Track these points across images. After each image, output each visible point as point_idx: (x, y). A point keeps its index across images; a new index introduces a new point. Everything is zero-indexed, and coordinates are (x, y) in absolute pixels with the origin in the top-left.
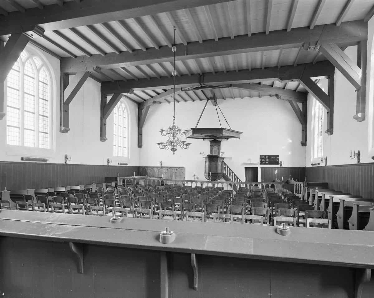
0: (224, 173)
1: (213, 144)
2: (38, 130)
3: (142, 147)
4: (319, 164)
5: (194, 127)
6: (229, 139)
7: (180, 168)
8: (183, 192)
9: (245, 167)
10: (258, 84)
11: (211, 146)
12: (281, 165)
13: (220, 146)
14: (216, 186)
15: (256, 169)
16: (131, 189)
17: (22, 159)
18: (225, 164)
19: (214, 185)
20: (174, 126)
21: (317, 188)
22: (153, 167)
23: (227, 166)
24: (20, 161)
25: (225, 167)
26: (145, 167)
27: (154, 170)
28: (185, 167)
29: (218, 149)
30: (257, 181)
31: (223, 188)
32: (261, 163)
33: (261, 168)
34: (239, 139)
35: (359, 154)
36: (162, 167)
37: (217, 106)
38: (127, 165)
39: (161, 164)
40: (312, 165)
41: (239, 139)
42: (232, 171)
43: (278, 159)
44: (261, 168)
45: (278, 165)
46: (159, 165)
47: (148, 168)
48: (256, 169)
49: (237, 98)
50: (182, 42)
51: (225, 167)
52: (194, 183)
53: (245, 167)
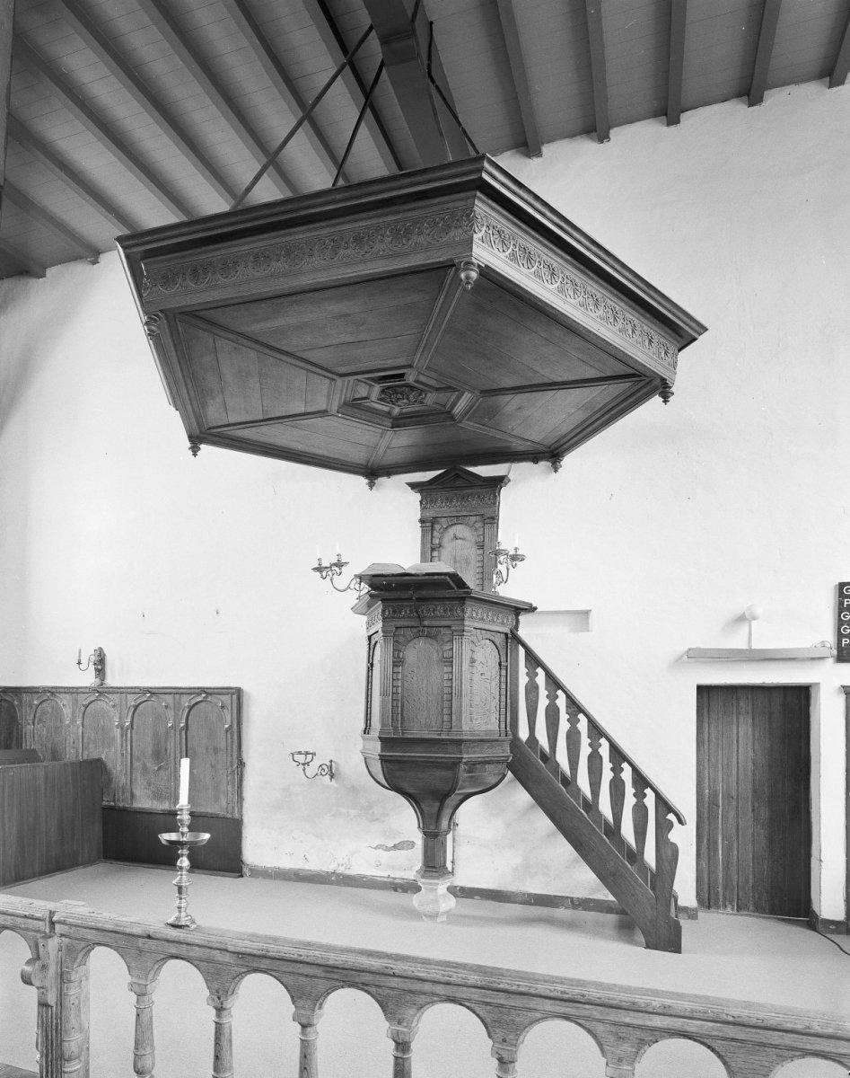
6: (382, 480)
36: (101, 691)
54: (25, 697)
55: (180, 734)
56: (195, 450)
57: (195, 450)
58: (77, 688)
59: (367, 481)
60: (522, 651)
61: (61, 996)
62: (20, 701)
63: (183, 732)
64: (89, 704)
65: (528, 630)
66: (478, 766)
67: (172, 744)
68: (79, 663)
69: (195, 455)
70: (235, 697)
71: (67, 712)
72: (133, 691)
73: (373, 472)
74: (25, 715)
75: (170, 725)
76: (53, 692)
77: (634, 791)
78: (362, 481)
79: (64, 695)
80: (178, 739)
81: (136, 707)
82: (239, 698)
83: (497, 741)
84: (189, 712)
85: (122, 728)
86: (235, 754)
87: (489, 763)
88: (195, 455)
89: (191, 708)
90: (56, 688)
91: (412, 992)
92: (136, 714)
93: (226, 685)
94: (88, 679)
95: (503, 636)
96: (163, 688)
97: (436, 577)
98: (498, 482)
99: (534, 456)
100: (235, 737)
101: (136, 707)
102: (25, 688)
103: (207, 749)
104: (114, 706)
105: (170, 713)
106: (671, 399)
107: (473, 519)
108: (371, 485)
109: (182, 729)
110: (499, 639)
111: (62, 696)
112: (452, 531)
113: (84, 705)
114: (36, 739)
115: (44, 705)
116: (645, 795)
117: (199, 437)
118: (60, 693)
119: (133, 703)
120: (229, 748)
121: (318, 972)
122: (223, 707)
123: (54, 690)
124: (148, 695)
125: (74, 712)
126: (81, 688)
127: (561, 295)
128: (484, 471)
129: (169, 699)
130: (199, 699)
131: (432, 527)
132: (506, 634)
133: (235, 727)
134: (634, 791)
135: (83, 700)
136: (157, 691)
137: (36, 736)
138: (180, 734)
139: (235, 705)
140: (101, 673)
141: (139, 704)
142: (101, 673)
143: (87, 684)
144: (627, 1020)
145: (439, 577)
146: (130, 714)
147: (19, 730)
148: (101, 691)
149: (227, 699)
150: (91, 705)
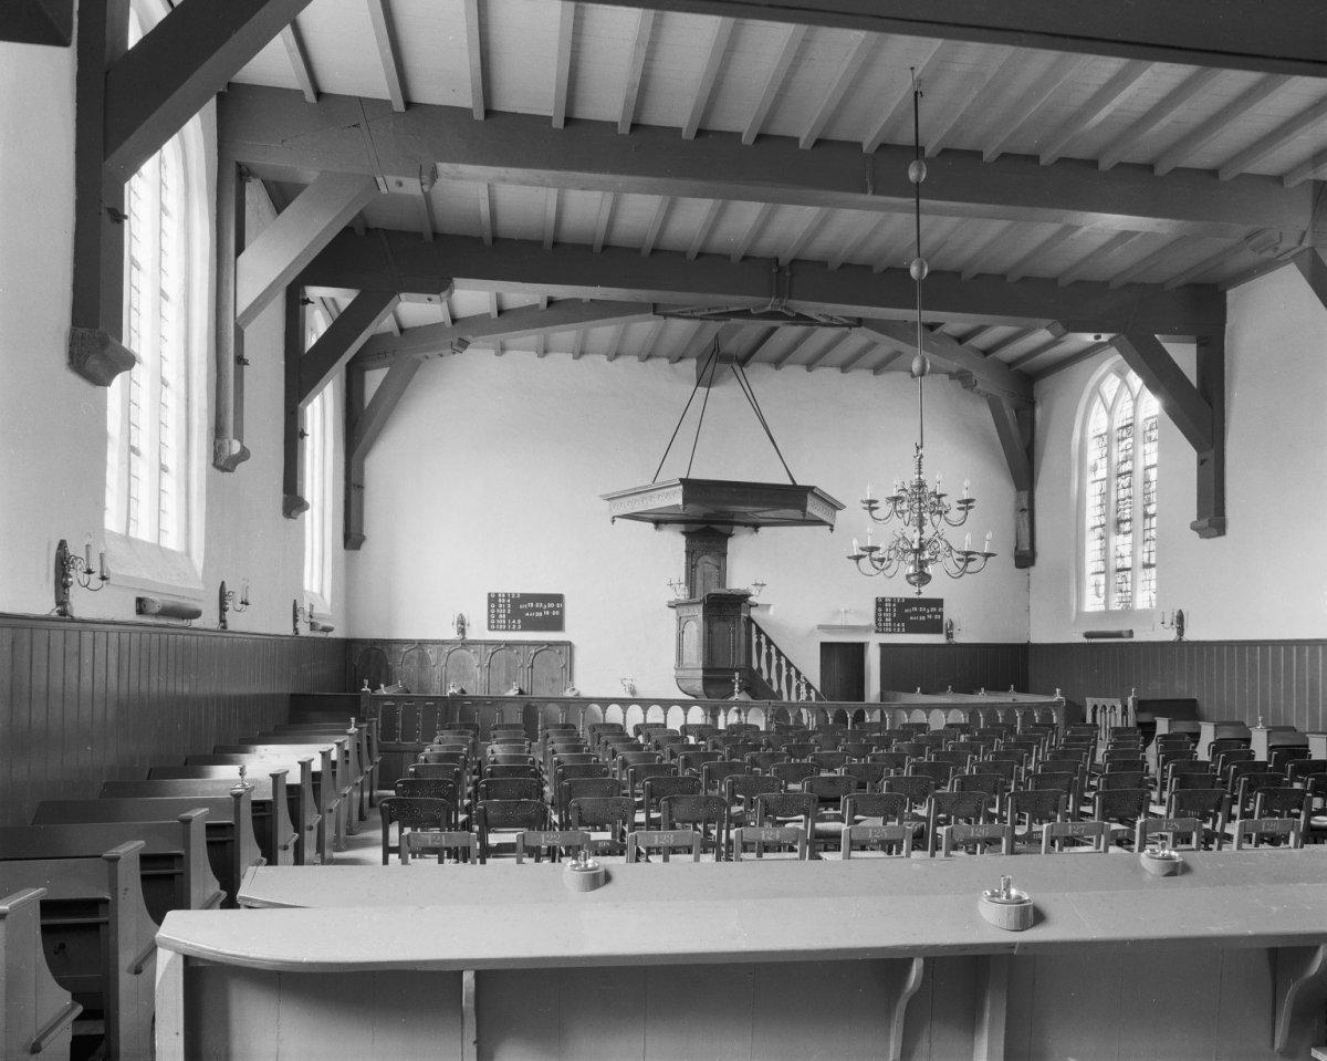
0: (755, 666)
1: (697, 543)
2: (160, 460)
3: (364, 546)
4: (1131, 633)
5: (685, 477)
6: (762, 529)
7: (554, 648)
8: (852, 750)
9: (823, 645)
10: (950, 336)
11: (690, 553)
12: (949, 636)
13: (725, 555)
14: (722, 722)
15: (859, 650)
16: (618, 748)
17: (141, 605)
18: (759, 631)
19: (715, 718)
20: (921, 485)
21: (353, 719)
22: (422, 643)
23: (767, 638)
24: (130, 614)
25: (759, 645)
26: (376, 641)
27: (423, 659)
28: (575, 642)
29: (719, 568)
30: (860, 696)
31: (1116, 731)
32: (880, 630)
33: (882, 646)
34: (832, 530)
35: (1180, 618)
36: (465, 644)
37: (702, 390)
38: (330, 635)
39: (462, 631)
40: (1088, 635)
41: (832, 530)
42: (787, 659)
43: (941, 614)
44: (882, 646)
45: (939, 636)
46: (452, 634)
47: (395, 647)
48: (859, 650)
49: (659, 360)
50: (389, 98)
51: (759, 645)
52: (676, 711)
53: (823, 645)
78: (652, 525)
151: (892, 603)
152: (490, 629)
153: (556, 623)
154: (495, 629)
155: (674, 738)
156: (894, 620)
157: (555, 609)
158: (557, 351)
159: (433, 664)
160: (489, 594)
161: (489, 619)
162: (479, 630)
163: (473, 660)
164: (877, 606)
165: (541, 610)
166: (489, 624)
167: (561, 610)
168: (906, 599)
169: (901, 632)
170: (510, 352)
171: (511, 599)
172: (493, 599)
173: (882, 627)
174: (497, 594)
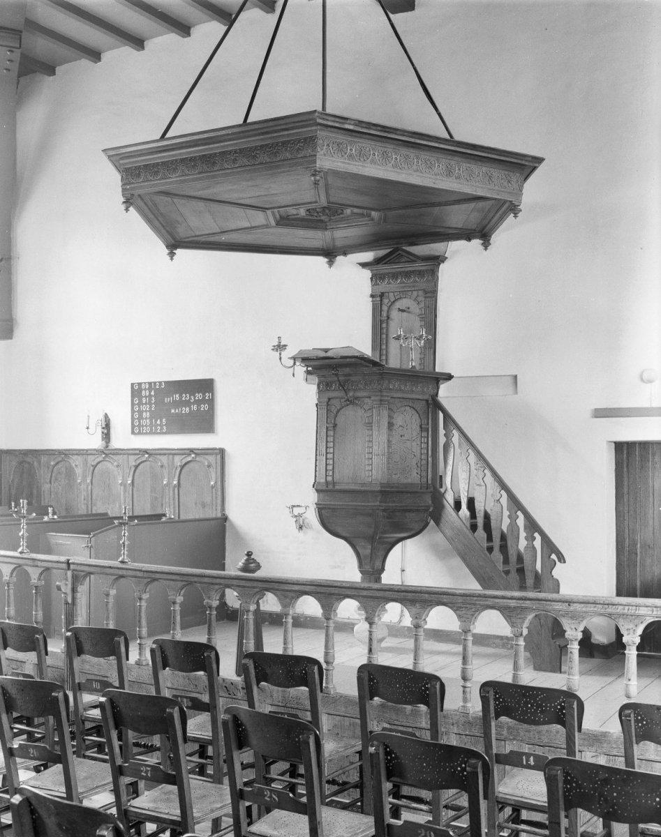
6: (340, 259)
36: (107, 452)
54: (44, 459)
55: (174, 490)
56: (172, 255)
57: (172, 255)
58: (87, 450)
59: (326, 260)
60: (441, 415)
61: (74, 598)
62: (39, 463)
63: (176, 489)
64: (97, 464)
65: (444, 392)
66: (397, 514)
67: (167, 500)
68: (88, 428)
69: (172, 259)
70: (219, 457)
71: (79, 471)
72: (133, 452)
73: (330, 254)
74: (43, 475)
75: (165, 483)
76: (65, 454)
77: (525, 535)
78: (322, 260)
79: (76, 456)
80: (171, 494)
81: (137, 467)
82: (223, 458)
83: (417, 492)
84: (181, 470)
85: (125, 486)
86: (219, 508)
87: (410, 511)
88: (172, 259)
89: (182, 467)
90: (69, 450)
91: (212, 584)
92: (137, 474)
93: (211, 447)
94: (96, 442)
95: (424, 402)
96: (158, 450)
97: (348, 360)
98: (438, 260)
99: (467, 235)
100: (219, 493)
101: (137, 467)
102: (42, 450)
103: (196, 504)
104: (118, 466)
105: (165, 472)
106: (519, 215)
107: (415, 293)
108: (331, 263)
109: (175, 486)
110: (420, 406)
111: (75, 457)
112: (398, 305)
113: (93, 466)
114: (53, 496)
115: (60, 466)
116: (534, 539)
117: (174, 245)
118: (73, 454)
119: (134, 464)
120: (214, 502)
121: (178, 578)
122: (209, 466)
123: (67, 452)
124: (147, 456)
125: (84, 471)
126: (91, 450)
127: (396, 170)
128: (421, 250)
129: (164, 459)
130: (189, 459)
131: (381, 300)
132: (427, 401)
133: (219, 483)
134: (525, 535)
135: (92, 460)
136: (154, 452)
137: (52, 494)
138: (174, 490)
139: (219, 462)
140: (107, 436)
141: (139, 464)
142: (107, 436)
143: (96, 446)
144: (286, 588)
145: (351, 360)
146: (132, 473)
147: (39, 489)
148: (107, 452)
149: (211, 459)
150: (99, 466)
151: (150, 389)
152: (133, 433)
153: (206, 423)
154: (139, 433)
155: (218, 612)
156: (154, 416)
157: (203, 401)
158: (152, 37)
159: (79, 481)
160: (132, 384)
161: (133, 419)
162: (123, 438)
163: (120, 476)
164: (133, 396)
165: (188, 403)
166: (133, 426)
167: (211, 402)
168: (166, 383)
169: (162, 433)
170: (197, 27)
171: (156, 390)
172: (136, 391)
173: (139, 426)
174: (140, 384)
